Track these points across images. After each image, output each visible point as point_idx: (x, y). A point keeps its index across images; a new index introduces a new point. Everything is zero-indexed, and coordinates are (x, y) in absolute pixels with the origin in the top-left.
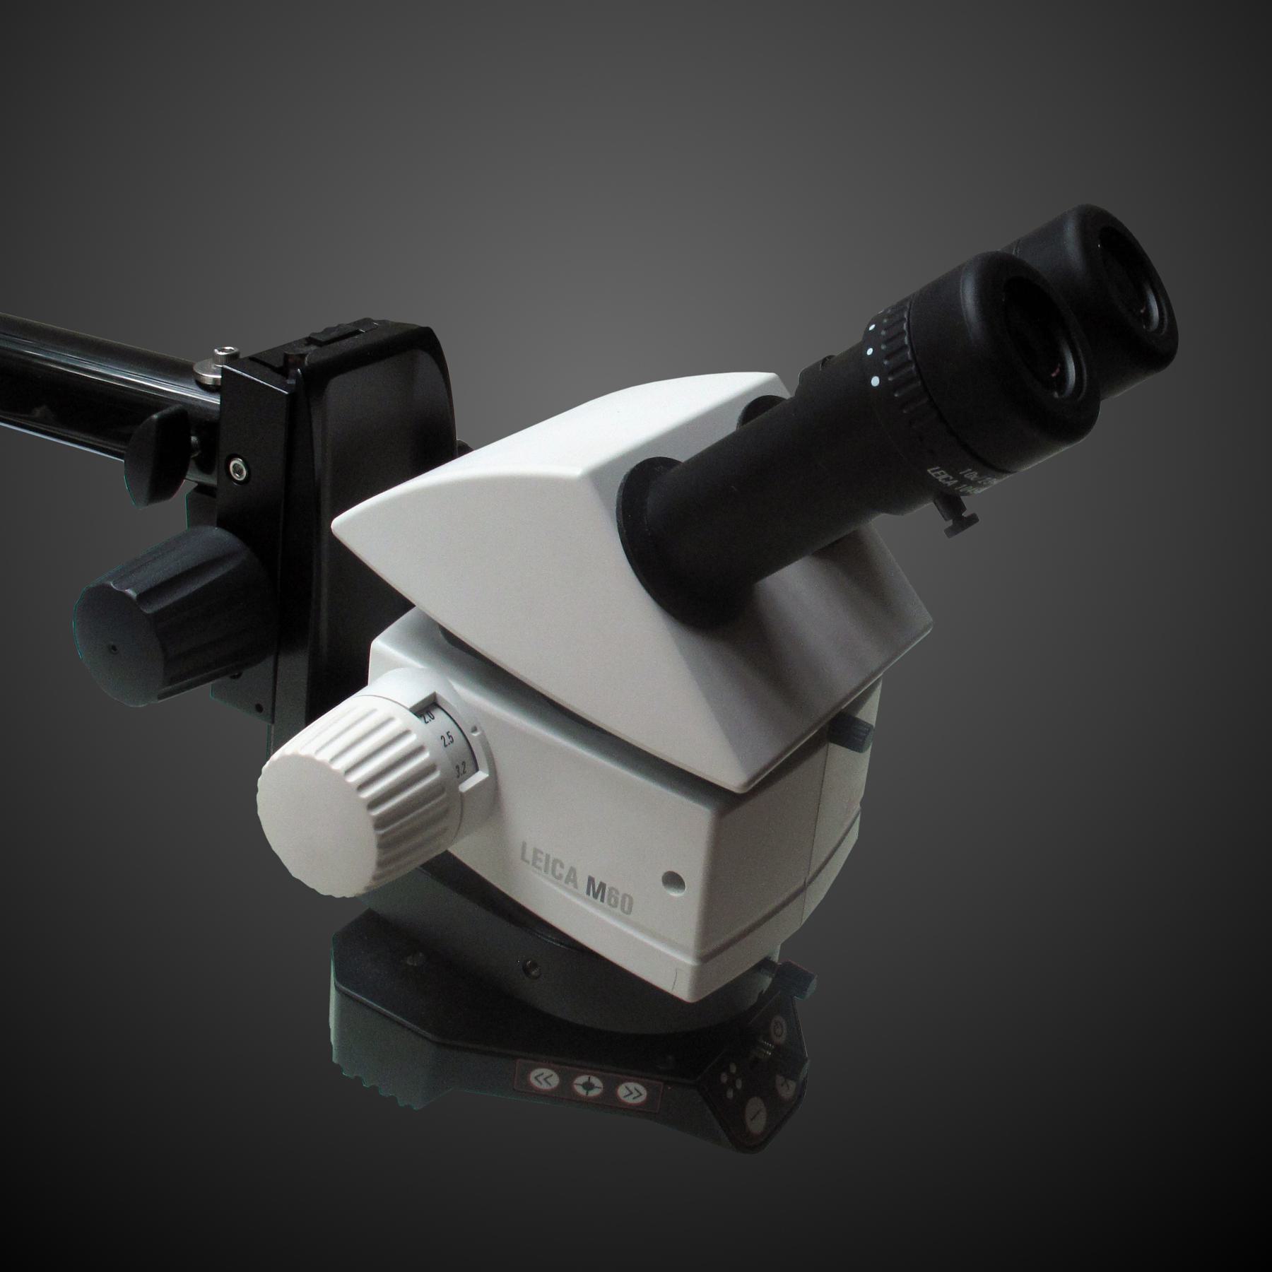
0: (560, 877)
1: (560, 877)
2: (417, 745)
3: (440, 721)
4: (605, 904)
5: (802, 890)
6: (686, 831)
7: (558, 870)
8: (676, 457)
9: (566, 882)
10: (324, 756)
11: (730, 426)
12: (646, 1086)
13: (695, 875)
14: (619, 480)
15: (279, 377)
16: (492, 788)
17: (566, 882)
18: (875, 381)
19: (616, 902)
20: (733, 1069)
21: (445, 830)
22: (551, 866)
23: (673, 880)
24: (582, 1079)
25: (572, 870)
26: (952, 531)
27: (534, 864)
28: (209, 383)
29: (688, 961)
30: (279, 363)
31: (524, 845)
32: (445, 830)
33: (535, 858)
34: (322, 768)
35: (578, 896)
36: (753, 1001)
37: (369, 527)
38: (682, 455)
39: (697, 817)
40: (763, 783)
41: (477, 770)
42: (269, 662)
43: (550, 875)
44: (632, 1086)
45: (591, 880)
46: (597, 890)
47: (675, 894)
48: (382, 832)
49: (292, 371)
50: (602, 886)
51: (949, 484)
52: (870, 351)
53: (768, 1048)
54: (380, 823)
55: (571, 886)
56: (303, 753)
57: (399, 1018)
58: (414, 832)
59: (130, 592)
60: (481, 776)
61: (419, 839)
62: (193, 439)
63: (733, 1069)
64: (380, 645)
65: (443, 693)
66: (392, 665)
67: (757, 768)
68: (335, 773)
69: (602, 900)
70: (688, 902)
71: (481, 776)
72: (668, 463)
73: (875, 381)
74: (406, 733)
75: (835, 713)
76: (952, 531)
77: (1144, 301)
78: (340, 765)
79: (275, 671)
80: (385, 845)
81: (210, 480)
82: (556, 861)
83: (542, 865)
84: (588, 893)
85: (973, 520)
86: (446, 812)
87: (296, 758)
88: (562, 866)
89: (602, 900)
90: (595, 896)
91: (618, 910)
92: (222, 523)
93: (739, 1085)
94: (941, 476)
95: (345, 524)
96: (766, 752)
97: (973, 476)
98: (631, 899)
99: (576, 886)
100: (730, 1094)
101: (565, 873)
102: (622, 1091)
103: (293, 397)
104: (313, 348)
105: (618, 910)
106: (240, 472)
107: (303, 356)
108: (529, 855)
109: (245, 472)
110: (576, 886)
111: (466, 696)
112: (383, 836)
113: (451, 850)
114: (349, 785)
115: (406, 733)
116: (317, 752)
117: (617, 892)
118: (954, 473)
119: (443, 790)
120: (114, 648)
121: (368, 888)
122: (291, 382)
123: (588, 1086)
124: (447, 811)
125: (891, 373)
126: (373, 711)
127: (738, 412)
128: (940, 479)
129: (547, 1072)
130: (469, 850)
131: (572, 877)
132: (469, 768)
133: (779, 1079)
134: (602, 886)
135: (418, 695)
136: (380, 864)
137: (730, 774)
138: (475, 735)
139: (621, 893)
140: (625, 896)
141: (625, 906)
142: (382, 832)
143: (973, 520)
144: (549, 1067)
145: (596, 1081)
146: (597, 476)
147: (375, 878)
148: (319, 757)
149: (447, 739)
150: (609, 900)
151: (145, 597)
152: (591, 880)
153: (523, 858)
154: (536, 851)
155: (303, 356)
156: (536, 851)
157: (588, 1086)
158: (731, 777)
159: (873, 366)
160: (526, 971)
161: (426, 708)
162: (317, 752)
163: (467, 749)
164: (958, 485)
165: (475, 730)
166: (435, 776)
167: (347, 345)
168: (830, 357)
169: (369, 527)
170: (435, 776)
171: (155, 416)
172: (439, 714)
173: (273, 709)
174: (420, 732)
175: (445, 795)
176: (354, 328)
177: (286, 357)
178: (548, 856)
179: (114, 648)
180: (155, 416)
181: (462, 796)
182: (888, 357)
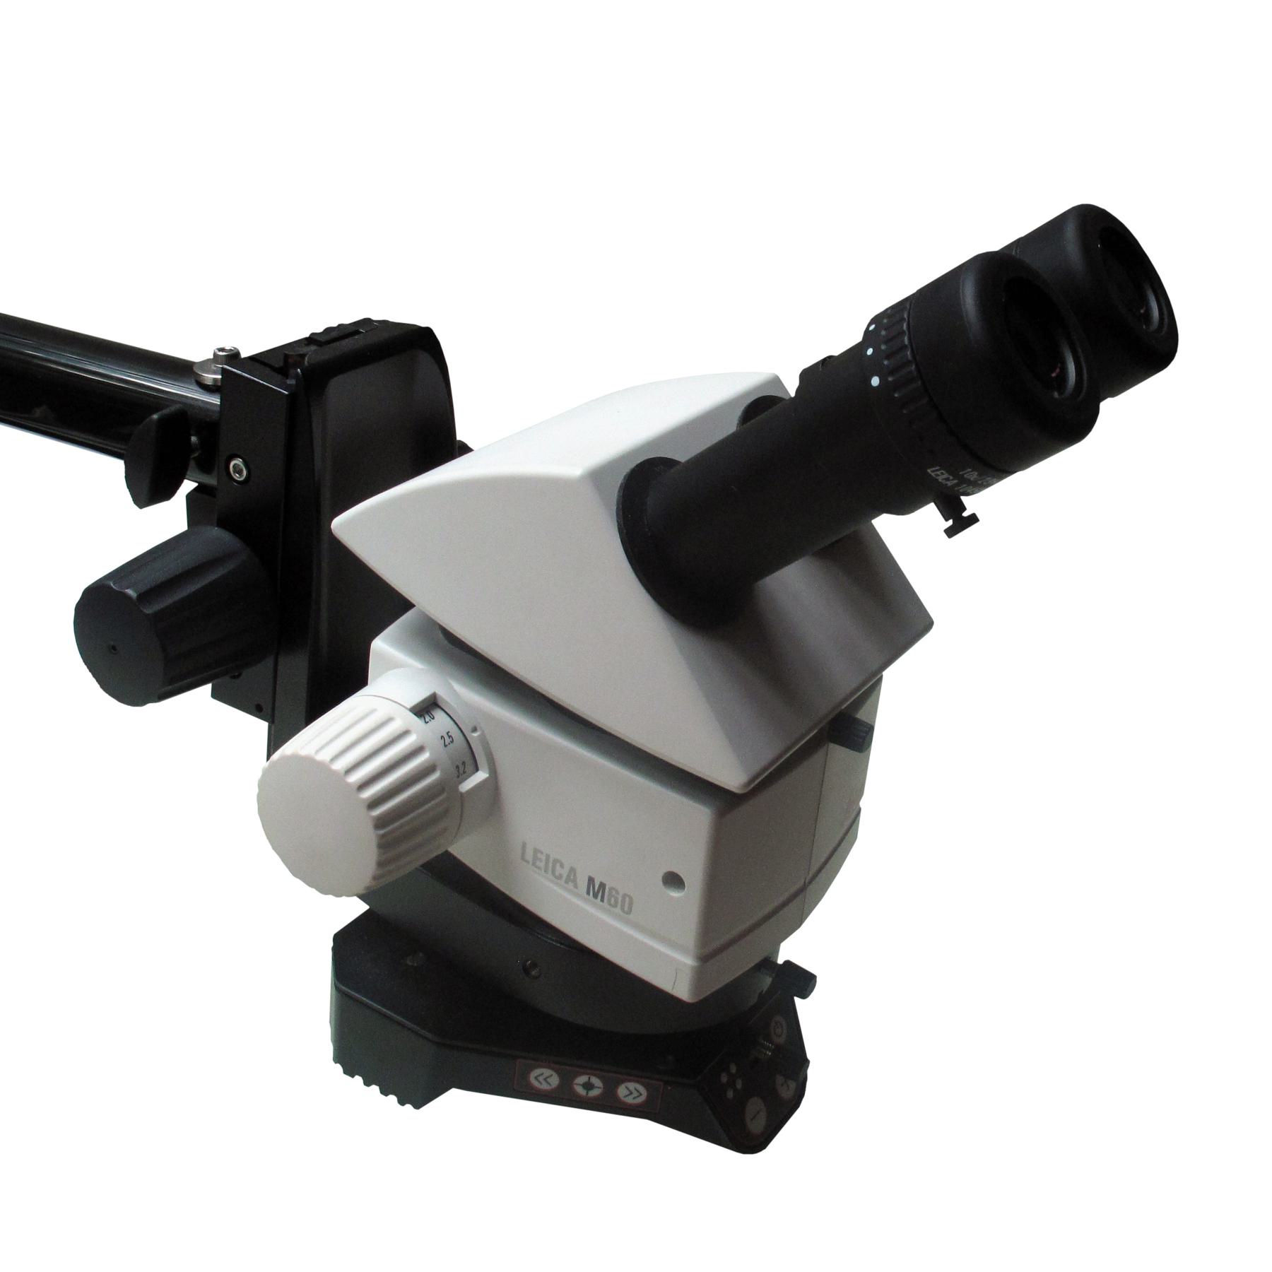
0: (560, 877)
1: (560, 877)
2: (417, 745)
3: (440, 721)
4: (605, 904)
5: (802, 890)
6: (686, 831)
7: (558, 870)
8: (676, 457)
9: (566, 882)
10: (324, 756)
11: (730, 426)
12: (646, 1086)
13: (695, 875)
14: (619, 480)
15: (279, 377)
16: (492, 788)
17: (566, 882)
18: (875, 381)
19: (616, 902)
20: (733, 1069)
21: (445, 830)
22: (551, 866)
23: (673, 880)
24: (582, 1079)
25: (572, 870)
26: (951, 532)
27: (534, 864)
28: (209, 383)
29: (688, 961)
30: (279, 363)
31: (524, 845)
32: (445, 830)
33: (535, 858)
34: (322, 768)
35: (578, 896)
36: (753, 1001)
37: (369, 527)
38: (682, 455)
39: (697, 817)
40: (763, 783)
41: (477, 770)
42: (269, 662)
43: (550, 875)
44: (632, 1086)
45: (591, 880)
46: (597, 890)
47: (675, 894)
48: (382, 832)
49: (292, 371)
50: (602, 886)
51: (949, 484)
52: (870, 351)
53: (768, 1048)
54: (380, 823)
55: (571, 886)
56: (303, 753)
57: (399, 1018)
58: (414, 832)
59: (130, 592)
60: (481, 776)
61: (419, 839)
62: (193, 439)
63: (733, 1069)
64: (380, 645)
65: (443, 693)
66: (392, 665)
67: (757, 768)
68: (335, 773)
69: (602, 900)
70: (688, 902)
71: (481, 776)
72: (668, 463)
73: (875, 381)
74: (406, 733)
75: (835, 713)
76: (951, 532)
77: (1144, 301)
78: (340, 765)
79: (275, 671)
80: (385, 845)
81: (211, 480)
82: (556, 861)
83: (542, 865)
84: (588, 893)
85: (973, 519)
86: (446, 812)
87: (296, 758)
88: (562, 866)
89: (602, 900)
90: (595, 896)
91: (618, 910)
92: (222, 523)
93: (739, 1085)
94: (941, 476)
95: (345, 524)
96: (766, 752)
97: (973, 476)
98: (631, 899)
99: (576, 886)
100: (730, 1094)
101: (565, 873)
102: (622, 1091)
103: (293, 397)
104: (313, 348)
105: (618, 910)
106: (240, 472)
107: (303, 356)
108: (529, 855)
109: (245, 472)
110: (576, 886)
111: (466, 696)
112: (383, 836)
113: (451, 850)
114: (349, 785)
115: (406, 733)
116: (317, 752)
117: (617, 892)
118: (954, 473)
119: (443, 790)
120: (114, 648)
121: (368, 888)
122: (291, 382)
123: (588, 1086)
124: (447, 811)
125: (891, 373)
126: (373, 711)
127: (738, 412)
128: (940, 479)
129: (547, 1072)
130: (469, 850)
131: (572, 877)
132: (469, 768)
133: (779, 1079)
134: (602, 886)
135: (418, 695)
136: (380, 864)
137: (730, 774)
138: (475, 735)
139: (621, 893)
140: (625, 896)
141: (625, 906)
142: (382, 832)
143: (973, 519)
144: (549, 1067)
145: (596, 1081)
146: (597, 476)
147: (375, 878)
148: (319, 757)
149: (447, 739)
150: (609, 900)
151: (145, 597)
152: (591, 880)
153: (523, 858)
154: (536, 851)
155: (303, 356)
156: (536, 851)
157: (588, 1086)
158: (731, 777)
159: (873, 366)
160: (526, 971)
161: (426, 708)
162: (317, 752)
163: (467, 749)
164: (958, 485)
165: (475, 730)
166: (435, 776)
167: (347, 345)
168: (830, 357)
169: (369, 527)
170: (435, 776)
171: (155, 416)
172: (439, 714)
173: (273, 709)
174: (420, 732)
175: (445, 795)
176: (354, 328)
177: (286, 357)
178: (548, 856)
179: (114, 648)
180: (155, 416)
181: (462, 796)
182: (888, 357)
